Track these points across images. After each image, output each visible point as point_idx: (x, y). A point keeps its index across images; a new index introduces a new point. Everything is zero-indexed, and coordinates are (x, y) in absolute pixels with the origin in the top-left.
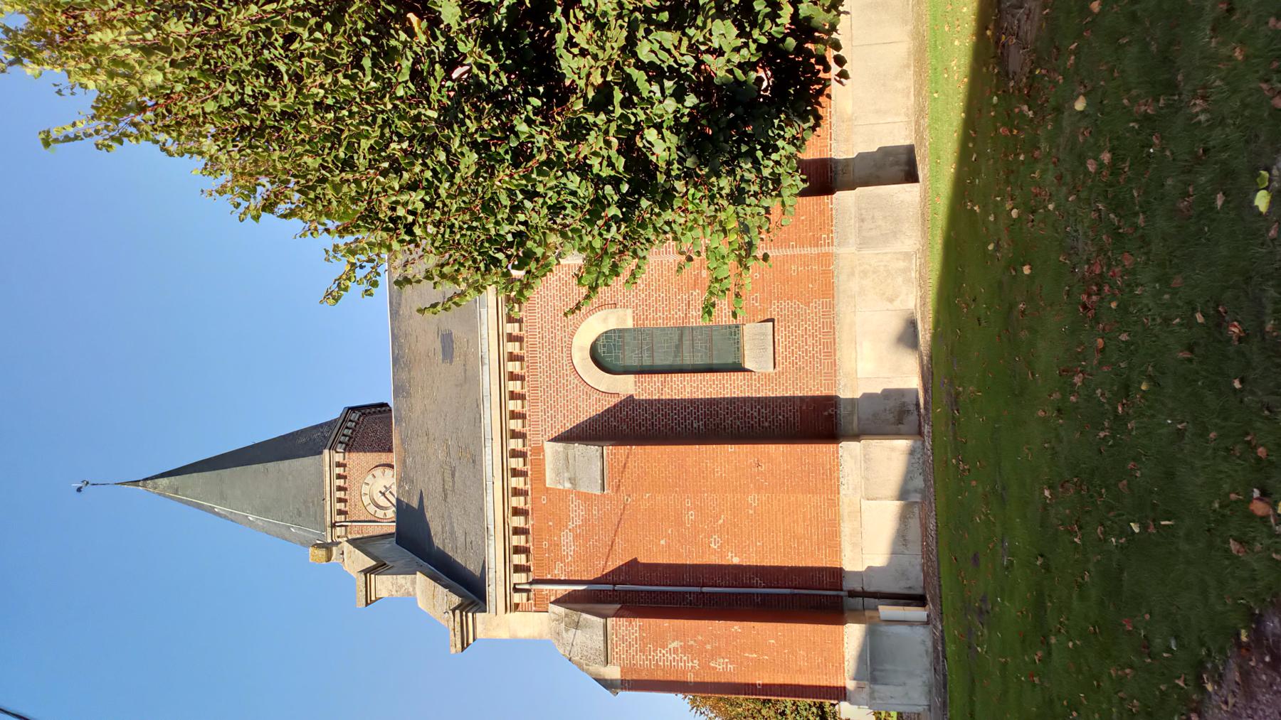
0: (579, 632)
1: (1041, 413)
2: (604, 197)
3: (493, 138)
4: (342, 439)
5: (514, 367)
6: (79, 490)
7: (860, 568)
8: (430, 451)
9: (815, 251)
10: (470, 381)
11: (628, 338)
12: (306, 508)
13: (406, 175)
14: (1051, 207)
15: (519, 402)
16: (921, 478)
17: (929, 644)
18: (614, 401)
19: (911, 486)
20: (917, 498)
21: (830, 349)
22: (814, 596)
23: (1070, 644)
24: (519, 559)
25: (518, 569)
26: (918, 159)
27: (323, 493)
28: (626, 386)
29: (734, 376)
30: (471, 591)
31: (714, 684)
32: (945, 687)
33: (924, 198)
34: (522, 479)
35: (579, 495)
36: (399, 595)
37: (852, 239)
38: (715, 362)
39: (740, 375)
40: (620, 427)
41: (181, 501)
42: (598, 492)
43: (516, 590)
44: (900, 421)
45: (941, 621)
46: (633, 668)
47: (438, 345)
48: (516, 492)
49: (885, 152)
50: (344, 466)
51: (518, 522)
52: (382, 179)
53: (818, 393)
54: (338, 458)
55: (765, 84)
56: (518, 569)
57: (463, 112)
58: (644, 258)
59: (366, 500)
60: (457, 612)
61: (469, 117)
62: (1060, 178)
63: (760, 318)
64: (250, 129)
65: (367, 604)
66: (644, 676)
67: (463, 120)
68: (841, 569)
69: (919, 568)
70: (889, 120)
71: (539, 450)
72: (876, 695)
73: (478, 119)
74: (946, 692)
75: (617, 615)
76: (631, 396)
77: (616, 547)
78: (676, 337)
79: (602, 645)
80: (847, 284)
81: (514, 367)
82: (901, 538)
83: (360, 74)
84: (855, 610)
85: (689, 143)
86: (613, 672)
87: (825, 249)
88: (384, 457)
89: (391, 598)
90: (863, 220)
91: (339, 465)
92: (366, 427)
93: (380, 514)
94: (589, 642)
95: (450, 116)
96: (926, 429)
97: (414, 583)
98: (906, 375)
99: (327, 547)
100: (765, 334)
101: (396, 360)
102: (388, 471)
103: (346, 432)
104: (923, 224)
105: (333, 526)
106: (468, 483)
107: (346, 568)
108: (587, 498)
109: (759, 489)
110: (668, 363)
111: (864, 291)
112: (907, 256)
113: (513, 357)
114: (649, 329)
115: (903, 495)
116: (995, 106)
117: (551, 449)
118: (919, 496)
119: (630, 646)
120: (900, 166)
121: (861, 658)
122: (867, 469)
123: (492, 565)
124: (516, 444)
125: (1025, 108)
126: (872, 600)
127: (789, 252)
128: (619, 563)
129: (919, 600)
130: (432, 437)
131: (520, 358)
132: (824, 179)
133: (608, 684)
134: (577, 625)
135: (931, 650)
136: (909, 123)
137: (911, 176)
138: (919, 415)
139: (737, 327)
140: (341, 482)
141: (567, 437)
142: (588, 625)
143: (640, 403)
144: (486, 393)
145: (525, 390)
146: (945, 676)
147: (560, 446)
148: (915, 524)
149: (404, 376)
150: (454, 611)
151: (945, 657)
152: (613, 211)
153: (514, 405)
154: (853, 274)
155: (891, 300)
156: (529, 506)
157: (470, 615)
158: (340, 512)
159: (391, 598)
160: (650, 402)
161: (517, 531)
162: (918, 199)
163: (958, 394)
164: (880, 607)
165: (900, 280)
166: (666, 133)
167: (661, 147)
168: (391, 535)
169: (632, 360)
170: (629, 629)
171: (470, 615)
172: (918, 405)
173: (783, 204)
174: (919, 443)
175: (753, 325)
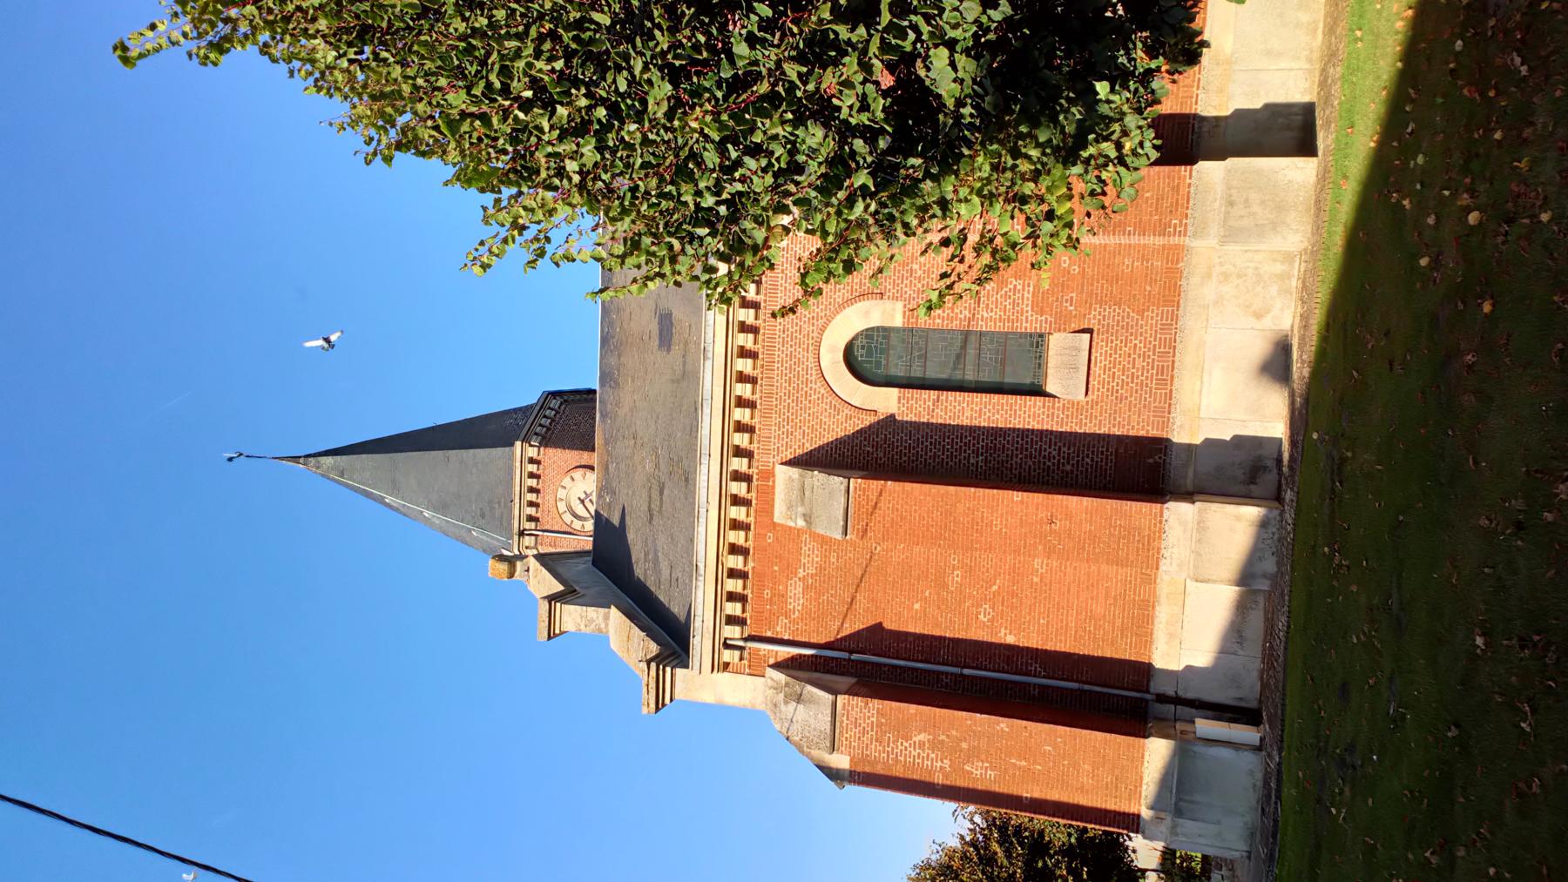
0: (801, 707)
1: (1484, 522)
2: (853, 153)
3: (694, 62)
5: (744, 365)
6: (230, 459)
7: (1176, 665)
8: (637, 459)
9: (1159, 241)
10: (688, 378)
11: (894, 340)
12: (493, 512)
13: (562, 111)
14: (1545, 217)
15: (748, 411)
16: (1274, 559)
17: (1259, 776)
18: (869, 420)
20: (1264, 585)
22: (1112, 695)
23: (1492, 871)
24: (734, 609)
25: (731, 620)
26: (1319, 122)
28: (887, 401)
29: (1030, 401)
30: (671, 639)
31: (968, 790)
32: (1274, 836)
33: (1323, 177)
34: (743, 509)
36: (588, 630)
37: (1215, 229)
39: (1039, 400)
41: (347, 486)
42: (838, 536)
43: (727, 646)
45: (1280, 750)
46: (865, 759)
47: (654, 327)
48: (736, 525)
49: (1273, 110)
50: (538, 462)
51: (735, 562)
52: (521, 115)
53: (1142, 433)
54: (532, 452)
56: (731, 620)
57: (652, 19)
59: (562, 507)
60: (653, 665)
63: (1075, 326)
65: (550, 637)
67: (651, 30)
68: (1150, 665)
69: (1255, 675)
70: (1283, 65)
71: (768, 475)
73: (673, 30)
74: (1274, 843)
75: (851, 692)
76: (893, 416)
77: (856, 606)
78: (958, 343)
79: (828, 727)
80: (1200, 290)
81: (744, 365)
82: (1235, 634)
86: (841, 761)
87: (1175, 240)
88: (585, 458)
90: (1231, 204)
91: (532, 461)
92: (566, 419)
93: (577, 525)
94: (812, 721)
96: (1288, 495)
97: (606, 618)
98: (1268, 417)
100: (1078, 349)
101: (605, 340)
102: (589, 473)
103: (543, 421)
105: (521, 533)
106: (678, 505)
107: (531, 589)
108: (824, 541)
109: (1049, 553)
110: (943, 376)
111: (1225, 298)
112: (1288, 258)
113: (744, 353)
114: (923, 330)
115: (1245, 578)
118: (1268, 582)
119: (864, 732)
120: (1288, 131)
121: (1164, 782)
123: (699, 612)
124: (739, 464)
125: (1518, 60)
126: (1187, 709)
127: (1124, 240)
128: (859, 626)
130: (639, 442)
131: (753, 355)
132: (1184, 141)
133: (834, 775)
134: (799, 699)
135: (1260, 784)
136: (1310, 71)
137: (1305, 146)
139: (1041, 336)
140: (533, 482)
142: (812, 701)
143: (904, 424)
144: (707, 395)
145: (757, 396)
146: (1276, 821)
147: (794, 472)
148: (1257, 619)
150: (649, 663)
151: (1278, 797)
152: (862, 178)
153: (742, 415)
154: (1209, 276)
155: (1259, 316)
156: (750, 544)
157: (668, 669)
158: (531, 518)
159: (578, 635)
161: (733, 573)
163: (1343, 460)
165: (1274, 289)
168: (586, 553)
169: (898, 371)
170: (863, 711)
171: (668, 669)
172: (1279, 460)
174: (1276, 512)
175: (1063, 335)
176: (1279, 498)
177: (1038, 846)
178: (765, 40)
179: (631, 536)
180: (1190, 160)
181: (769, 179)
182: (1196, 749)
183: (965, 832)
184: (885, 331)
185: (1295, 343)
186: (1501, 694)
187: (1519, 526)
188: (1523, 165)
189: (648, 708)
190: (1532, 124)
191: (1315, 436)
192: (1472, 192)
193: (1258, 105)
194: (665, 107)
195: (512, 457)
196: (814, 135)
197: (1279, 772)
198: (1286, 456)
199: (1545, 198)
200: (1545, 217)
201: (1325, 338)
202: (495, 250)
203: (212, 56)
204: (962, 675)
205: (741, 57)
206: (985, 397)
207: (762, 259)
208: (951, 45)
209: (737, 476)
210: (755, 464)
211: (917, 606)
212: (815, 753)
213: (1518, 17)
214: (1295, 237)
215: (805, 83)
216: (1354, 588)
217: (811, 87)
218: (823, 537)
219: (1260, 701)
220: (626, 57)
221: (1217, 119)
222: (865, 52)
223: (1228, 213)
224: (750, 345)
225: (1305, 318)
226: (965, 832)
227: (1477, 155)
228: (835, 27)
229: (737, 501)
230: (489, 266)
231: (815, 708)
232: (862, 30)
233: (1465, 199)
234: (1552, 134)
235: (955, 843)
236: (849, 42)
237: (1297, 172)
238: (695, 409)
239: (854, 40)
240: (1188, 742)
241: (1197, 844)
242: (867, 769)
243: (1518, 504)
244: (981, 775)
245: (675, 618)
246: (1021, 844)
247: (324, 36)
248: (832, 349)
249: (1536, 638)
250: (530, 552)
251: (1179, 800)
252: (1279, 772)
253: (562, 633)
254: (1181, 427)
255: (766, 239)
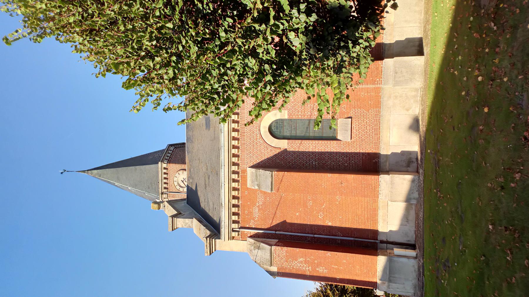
1: (489, 185)
2: (264, 70)
4: (167, 158)
6: (62, 173)
9: (373, 86)
11: (285, 124)
14: (505, 80)
15: (237, 150)
16: (417, 193)
17: (416, 267)
18: (278, 151)
19: (412, 196)
20: (414, 202)
21: (377, 130)
22: (365, 242)
24: (235, 218)
25: (234, 222)
26: (424, 44)
27: (158, 180)
28: (284, 145)
29: (332, 142)
30: (214, 229)
32: (423, 288)
33: (426, 63)
34: (237, 183)
35: (261, 192)
36: (186, 227)
38: (324, 135)
39: (335, 142)
40: (280, 163)
42: (270, 192)
43: (233, 231)
44: (408, 166)
45: (423, 258)
48: (235, 189)
49: (408, 40)
51: (235, 202)
52: (141, 61)
53: (370, 151)
54: (165, 165)
55: (354, 9)
56: (234, 222)
57: (188, 25)
58: (288, 97)
59: (176, 184)
60: (208, 239)
61: (191, 28)
62: (513, 65)
63: (346, 116)
64: (92, 32)
65: (173, 230)
66: (287, 271)
68: (377, 230)
69: (413, 232)
70: (411, 25)
71: (245, 171)
72: (390, 287)
74: (423, 290)
75: (276, 245)
76: (286, 149)
77: (277, 215)
78: (307, 123)
79: (269, 258)
80: (387, 102)
82: (406, 218)
83: (134, 3)
84: (382, 249)
85: (313, 41)
86: (274, 269)
89: (183, 228)
90: (396, 73)
91: (165, 168)
92: (176, 153)
93: (181, 189)
94: (263, 256)
95: (182, 28)
96: (421, 171)
97: (192, 222)
98: (413, 144)
99: (159, 204)
103: (168, 155)
104: (425, 76)
105: (162, 193)
107: (166, 213)
108: (265, 193)
110: (303, 135)
111: (394, 103)
112: (416, 90)
114: (295, 120)
115: (408, 200)
116: (471, 22)
117: (250, 172)
118: (416, 201)
120: (416, 48)
122: (392, 188)
123: (223, 219)
124: (235, 168)
125: (493, 24)
126: (391, 245)
128: (278, 222)
129: (412, 247)
132: (379, 53)
133: (272, 274)
134: (259, 248)
135: (417, 270)
137: (420, 53)
138: (418, 164)
140: (165, 176)
141: (257, 166)
142: (263, 249)
143: (290, 152)
144: (222, 145)
145: (240, 145)
146: (423, 283)
147: (253, 170)
148: (413, 213)
149: (190, 133)
150: (207, 238)
151: (423, 275)
152: (269, 78)
154: (390, 97)
155: (408, 110)
156: (240, 195)
157: (214, 240)
158: (165, 188)
159: (182, 228)
160: (294, 152)
162: (423, 63)
163: (439, 160)
164: (395, 249)
166: (301, 36)
167: (297, 42)
168: (185, 199)
169: (287, 134)
171: (214, 240)
172: (417, 159)
173: (360, 73)
174: (417, 177)
175: (342, 119)
176: (418, 172)
177: (344, 291)
178: (230, 31)
179: (199, 193)
180: (382, 59)
181: (236, 78)
182: (395, 259)
183: (318, 287)
184: (282, 121)
185: (420, 118)
186: (499, 246)
187: (502, 188)
188: (497, 61)
189: (207, 254)
190: (499, 47)
191: (429, 151)
192: (479, 69)
193: (403, 39)
194: (195, 55)
195: (158, 168)
196: (252, 62)
197: (423, 267)
198: (419, 157)
199: (505, 73)
200: (505, 80)
201: (430, 118)
202: (142, 104)
203: (38, 39)
204: (314, 237)
205: (223, 37)
206: (317, 142)
207: (235, 105)
208: (296, 30)
209: (234, 172)
210: (240, 168)
211: (297, 214)
212: (265, 266)
213: (492, 9)
214: (418, 83)
215: (245, 46)
216: (445, 205)
217: (247, 47)
218: (264, 192)
219: (415, 241)
220: (179, 39)
221: (390, 44)
222: (265, 34)
223: (395, 76)
224: (236, 127)
225: (423, 111)
226: (318, 287)
227: (480, 57)
228: (253, 25)
229: (234, 181)
230: (140, 110)
231: (264, 251)
232: (264, 26)
233: (476, 73)
234: (506, 51)
235: (315, 291)
236: (260, 30)
237: (418, 61)
238: (219, 150)
239: (261, 29)
240: (392, 257)
241: (396, 289)
242: (283, 271)
243: (501, 180)
244: (322, 271)
245: (215, 221)
246: (338, 290)
247: (77, 33)
248: (265, 127)
249: (511, 228)
250: (165, 200)
251: (390, 277)
252: (423, 267)
253: (177, 228)
254: (383, 149)
255: (237, 98)
